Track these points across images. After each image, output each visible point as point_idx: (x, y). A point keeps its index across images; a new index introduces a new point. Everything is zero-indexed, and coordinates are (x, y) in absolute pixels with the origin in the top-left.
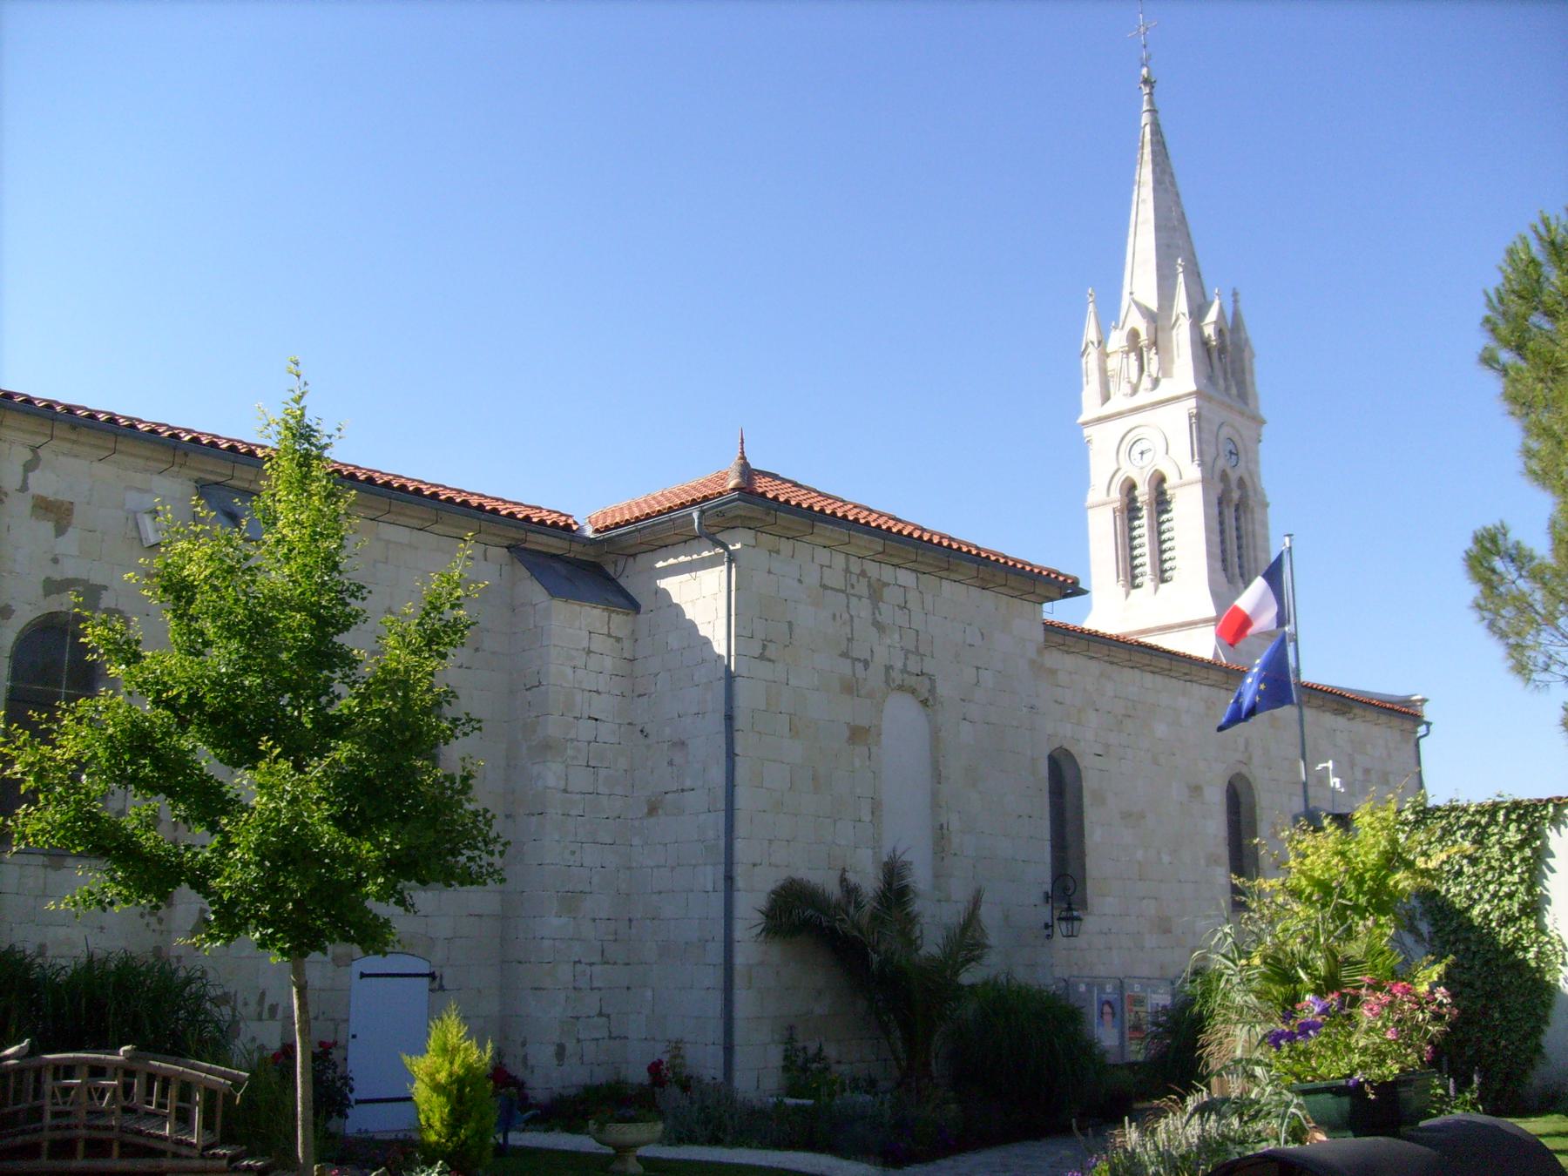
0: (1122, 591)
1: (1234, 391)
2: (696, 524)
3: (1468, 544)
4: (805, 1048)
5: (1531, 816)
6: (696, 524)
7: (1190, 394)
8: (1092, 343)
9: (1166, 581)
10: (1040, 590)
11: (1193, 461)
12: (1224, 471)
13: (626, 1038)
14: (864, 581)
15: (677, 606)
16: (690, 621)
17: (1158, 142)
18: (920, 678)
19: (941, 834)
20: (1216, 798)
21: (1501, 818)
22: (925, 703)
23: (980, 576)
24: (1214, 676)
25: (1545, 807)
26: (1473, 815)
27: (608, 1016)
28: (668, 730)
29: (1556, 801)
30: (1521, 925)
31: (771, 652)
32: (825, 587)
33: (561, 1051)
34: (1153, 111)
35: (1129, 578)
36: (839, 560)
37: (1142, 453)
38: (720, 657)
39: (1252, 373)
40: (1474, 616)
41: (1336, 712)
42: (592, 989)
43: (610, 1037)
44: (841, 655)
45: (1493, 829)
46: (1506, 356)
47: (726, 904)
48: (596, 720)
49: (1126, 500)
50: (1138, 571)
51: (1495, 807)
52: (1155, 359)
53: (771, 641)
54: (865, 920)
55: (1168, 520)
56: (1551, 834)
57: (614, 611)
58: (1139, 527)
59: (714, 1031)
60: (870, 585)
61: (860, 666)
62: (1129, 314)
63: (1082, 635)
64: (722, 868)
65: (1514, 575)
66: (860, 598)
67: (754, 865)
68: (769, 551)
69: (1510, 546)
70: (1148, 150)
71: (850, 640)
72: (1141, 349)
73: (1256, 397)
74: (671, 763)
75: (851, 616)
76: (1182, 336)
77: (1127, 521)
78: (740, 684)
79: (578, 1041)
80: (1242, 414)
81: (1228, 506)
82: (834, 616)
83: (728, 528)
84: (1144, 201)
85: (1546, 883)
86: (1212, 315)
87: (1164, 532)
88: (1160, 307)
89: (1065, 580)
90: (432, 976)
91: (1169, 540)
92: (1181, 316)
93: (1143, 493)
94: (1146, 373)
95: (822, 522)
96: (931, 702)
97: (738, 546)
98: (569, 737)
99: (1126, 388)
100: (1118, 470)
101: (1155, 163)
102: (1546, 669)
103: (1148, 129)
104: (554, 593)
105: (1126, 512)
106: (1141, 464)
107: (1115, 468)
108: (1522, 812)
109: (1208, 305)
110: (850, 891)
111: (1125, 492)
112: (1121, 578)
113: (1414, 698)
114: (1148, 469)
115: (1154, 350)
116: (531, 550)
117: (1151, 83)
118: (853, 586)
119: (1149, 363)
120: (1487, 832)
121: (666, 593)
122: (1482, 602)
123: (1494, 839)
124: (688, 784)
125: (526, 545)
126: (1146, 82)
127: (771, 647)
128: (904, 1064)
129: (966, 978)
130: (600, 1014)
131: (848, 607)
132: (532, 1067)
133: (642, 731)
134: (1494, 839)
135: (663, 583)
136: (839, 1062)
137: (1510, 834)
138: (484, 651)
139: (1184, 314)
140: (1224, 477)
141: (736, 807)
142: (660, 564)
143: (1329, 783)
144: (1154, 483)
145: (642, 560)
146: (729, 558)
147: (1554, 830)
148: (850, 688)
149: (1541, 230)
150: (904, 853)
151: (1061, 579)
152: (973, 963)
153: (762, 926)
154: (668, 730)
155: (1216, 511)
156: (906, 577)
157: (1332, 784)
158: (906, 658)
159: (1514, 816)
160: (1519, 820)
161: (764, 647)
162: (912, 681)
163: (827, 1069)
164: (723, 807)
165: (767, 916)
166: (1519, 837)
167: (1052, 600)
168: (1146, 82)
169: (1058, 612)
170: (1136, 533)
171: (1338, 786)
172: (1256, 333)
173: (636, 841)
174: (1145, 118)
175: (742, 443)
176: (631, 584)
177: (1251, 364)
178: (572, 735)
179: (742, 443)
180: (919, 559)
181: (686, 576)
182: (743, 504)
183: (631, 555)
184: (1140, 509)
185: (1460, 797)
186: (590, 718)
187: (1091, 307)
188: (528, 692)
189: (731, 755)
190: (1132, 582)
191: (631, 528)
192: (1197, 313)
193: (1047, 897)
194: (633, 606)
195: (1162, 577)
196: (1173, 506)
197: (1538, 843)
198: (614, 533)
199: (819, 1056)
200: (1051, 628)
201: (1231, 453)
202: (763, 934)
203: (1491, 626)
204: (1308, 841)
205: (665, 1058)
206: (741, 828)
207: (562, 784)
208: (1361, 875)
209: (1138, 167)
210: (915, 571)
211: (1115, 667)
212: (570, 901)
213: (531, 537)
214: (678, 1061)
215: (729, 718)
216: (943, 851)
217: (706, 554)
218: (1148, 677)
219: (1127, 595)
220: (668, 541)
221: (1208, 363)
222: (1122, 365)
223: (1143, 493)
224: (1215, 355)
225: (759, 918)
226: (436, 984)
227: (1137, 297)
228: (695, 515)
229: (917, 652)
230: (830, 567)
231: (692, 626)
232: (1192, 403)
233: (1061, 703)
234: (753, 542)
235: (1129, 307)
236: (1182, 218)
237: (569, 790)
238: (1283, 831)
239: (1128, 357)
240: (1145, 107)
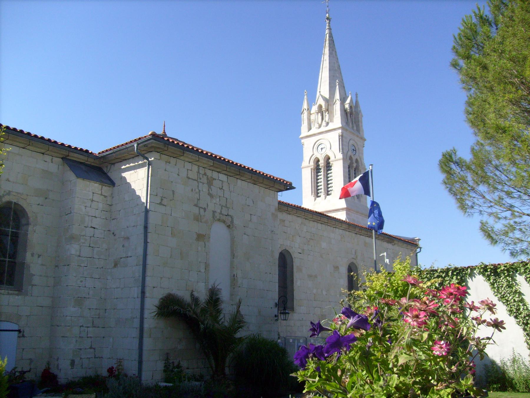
0: (313, 198)
1: (355, 128)
2: (136, 149)
3: (440, 157)
4: (173, 363)
5: (461, 274)
6: (136, 149)
7: (339, 128)
8: (305, 109)
9: (329, 195)
10: (277, 186)
11: (340, 152)
12: (351, 156)
13: (102, 357)
14: (205, 177)
15: (129, 183)
16: (133, 189)
17: (331, 40)
18: (227, 217)
19: (234, 278)
20: (344, 270)
21: (450, 274)
22: (229, 227)
23: (253, 178)
24: (344, 226)
25: (467, 270)
26: (439, 273)
27: (94, 349)
28: (123, 233)
29: (471, 267)
30: (457, 316)
31: (165, 202)
32: (189, 178)
33: (73, 363)
34: (330, 29)
36: (195, 168)
37: (322, 149)
38: (143, 203)
39: (362, 123)
40: (443, 187)
41: (388, 242)
42: (88, 337)
43: (95, 357)
44: (194, 206)
45: (447, 278)
46: (462, 63)
47: (141, 304)
48: (94, 228)
50: (319, 191)
51: (448, 270)
52: (327, 115)
53: (165, 198)
54: (199, 311)
55: (330, 173)
56: (469, 280)
57: (104, 185)
58: (320, 175)
59: (136, 356)
60: (208, 179)
61: (202, 211)
62: (319, 99)
63: (294, 207)
64: (140, 288)
65: (459, 170)
66: (203, 183)
67: (154, 287)
68: (166, 162)
69: (457, 158)
70: (327, 42)
71: (199, 200)
72: (323, 112)
73: (363, 131)
74: (123, 246)
75: (200, 191)
76: (337, 107)
77: (316, 174)
78: (151, 215)
79: (81, 358)
80: (358, 136)
81: (352, 169)
82: (192, 190)
83: (149, 152)
84: (325, 60)
85: (467, 300)
86: (348, 101)
87: (329, 177)
88: (330, 97)
89: (287, 183)
90: (19, 331)
91: (330, 180)
92: (337, 100)
93: (322, 163)
94: (324, 120)
95: (188, 151)
96: (231, 227)
97: (153, 159)
98: (82, 234)
99: (317, 126)
102: (472, 207)
103: (328, 35)
104: (78, 176)
106: (321, 153)
107: (312, 154)
108: (458, 272)
109: (348, 97)
110: (195, 300)
111: (315, 163)
112: (313, 194)
113: (416, 239)
114: (323, 155)
115: (327, 113)
116: (71, 160)
117: (330, 19)
118: (200, 179)
119: (325, 117)
120: (445, 280)
121: (125, 178)
122: (446, 181)
123: (447, 282)
124: (129, 254)
125: (68, 158)
126: (328, 19)
127: (165, 200)
128: (214, 369)
129: (238, 335)
130: (91, 348)
131: (198, 186)
132: (60, 369)
133: (113, 233)
134: (447, 282)
135: (124, 175)
136: (188, 368)
137: (453, 280)
138: (49, 199)
139: (338, 100)
140: (351, 158)
141: (147, 264)
142: (123, 167)
143: (385, 261)
145: (117, 165)
146: (148, 163)
147: (470, 279)
148: (198, 218)
149: (477, 12)
150: (218, 285)
151: (285, 182)
152: (240, 329)
153: (157, 312)
154: (123, 233)
155: (347, 170)
156: (223, 177)
157: (386, 262)
158: (222, 209)
159: (455, 273)
160: (457, 275)
161: (162, 200)
162: (224, 218)
163: (181, 371)
164: (142, 264)
165: (158, 308)
166: (457, 281)
167: (281, 191)
168: (328, 19)
169: (285, 197)
170: (319, 177)
171: (388, 262)
172: (363, 108)
173: (109, 278)
174: (327, 31)
175: (164, 127)
176: (112, 175)
177: (361, 118)
178: (83, 233)
179: (164, 127)
180: (228, 170)
181: (133, 171)
182: (154, 141)
183: (113, 164)
184: (320, 169)
185: (435, 266)
186: (91, 227)
187: (305, 97)
188: (67, 216)
189: (146, 242)
190: (317, 195)
191: (111, 152)
192: (343, 100)
193: (276, 305)
194: (112, 183)
195: (328, 193)
196: (332, 168)
197: (464, 284)
198: (105, 154)
199: (178, 366)
200: (280, 203)
201: (353, 150)
202: (157, 316)
203: (450, 190)
204: (374, 277)
205: (115, 366)
206: (149, 273)
207: (78, 253)
208: (397, 289)
209: (324, 48)
210: (227, 175)
211: (307, 220)
212: (79, 301)
213: (71, 154)
214: (120, 367)
215: (146, 228)
216: (235, 285)
217: (140, 162)
218: (319, 225)
219: (315, 200)
220: (127, 158)
221: (346, 117)
222: (316, 117)
223: (322, 163)
224: (349, 115)
225: (155, 309)
226: (21, 335)
227: (322, 93)
228: (135, 146)
229: (226, 207)
230: (191, 170)
231: (134, 191)
232: (340, 131)
233: (285, 233)
234: (159, 158)
235: (319, 96)
237: (81, 256)
238: (364, 272)
239: (318, 115)
240: (327, 28)
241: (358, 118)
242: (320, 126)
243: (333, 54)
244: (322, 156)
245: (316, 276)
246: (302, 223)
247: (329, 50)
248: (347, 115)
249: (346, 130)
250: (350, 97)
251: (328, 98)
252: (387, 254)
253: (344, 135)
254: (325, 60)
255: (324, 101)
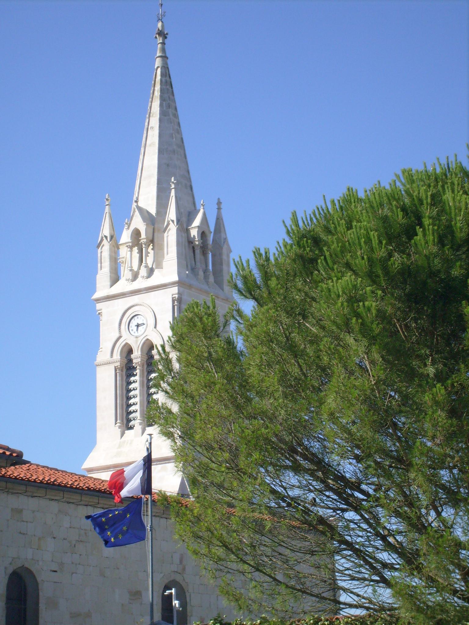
0: (118, 431)
7: (173, 284)
17: (166, 82)
34: (164, 57)
35: (125, 421)
37: (138, 326)
49: (125, 361)
50: (131, 416)
58: (134, 382)
63: (42, 485)
70: (158, 87)
77: (125, 378)
84: (152, 128)
86: (197, 222)
88: (158, 212)
92: (171, 222)
93: (137, 357)
94: (143, 264)
100: (120, 337)
101: (162, 99)
105: (125, 370)
106: (136, 334)
107: (117, 335)
109: (197, 212)
112: (118, 421)
114: (140, 339)
115: (151, 247)
139: (173, 221)
144: (146, 350)
157: (174, 604)
168: (161, 33)
170: (131, 386)
171: (177, 606)
174: (158, 62)
184: (135, 368)
187: (107, 209)
190: (127, 425)
211: (71, 505)
219: (122, 434)
223: (137, 357)
224: (198, 252)
227: (140, 204)
232: (175, 290)
236: (181, 144)
239: (131, 251)
240: (159, 54)
241: (221, 254)
242: (135, 276)
243: (169, 116)
244: (137, 341)
245: (88, 615)
246: (60, 511)
247: (161, 105)
248: (194, 251)
249: (190, 287)
250: (202, 211)
251: (154, 215)
252: (176, 592)
253: (184, 297)
254: (152, 128)
255: (144, 221)
